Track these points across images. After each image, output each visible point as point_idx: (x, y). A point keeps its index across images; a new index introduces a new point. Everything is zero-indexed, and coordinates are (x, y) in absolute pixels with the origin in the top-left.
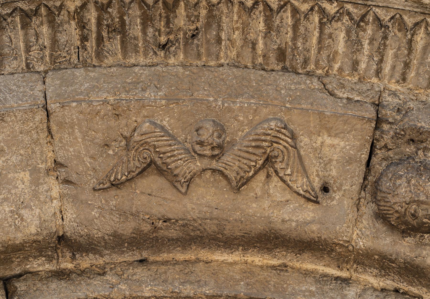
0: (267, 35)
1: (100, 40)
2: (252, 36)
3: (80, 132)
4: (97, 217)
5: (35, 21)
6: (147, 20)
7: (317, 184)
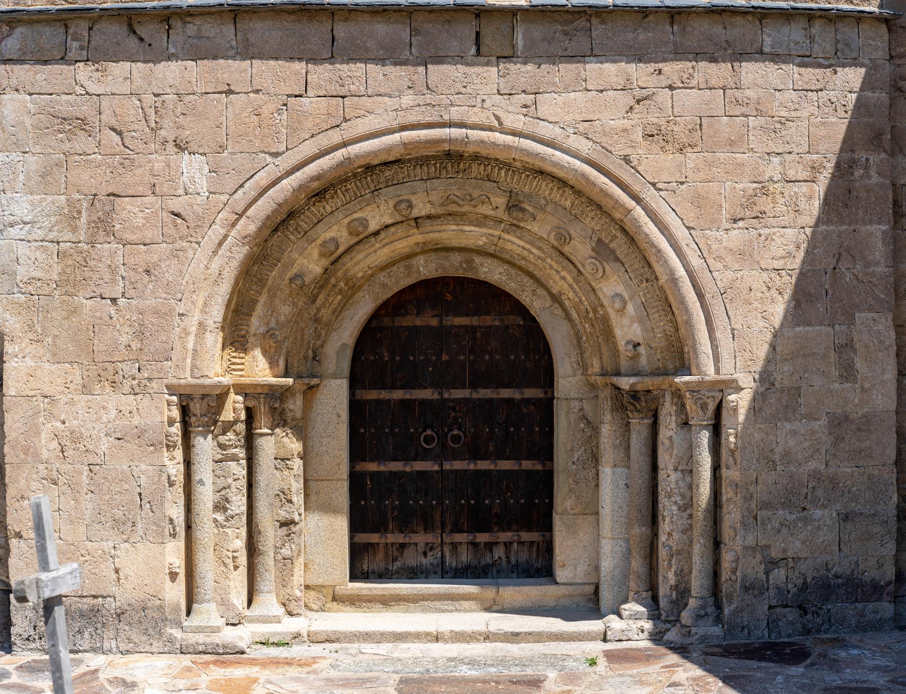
6: (452, 167)
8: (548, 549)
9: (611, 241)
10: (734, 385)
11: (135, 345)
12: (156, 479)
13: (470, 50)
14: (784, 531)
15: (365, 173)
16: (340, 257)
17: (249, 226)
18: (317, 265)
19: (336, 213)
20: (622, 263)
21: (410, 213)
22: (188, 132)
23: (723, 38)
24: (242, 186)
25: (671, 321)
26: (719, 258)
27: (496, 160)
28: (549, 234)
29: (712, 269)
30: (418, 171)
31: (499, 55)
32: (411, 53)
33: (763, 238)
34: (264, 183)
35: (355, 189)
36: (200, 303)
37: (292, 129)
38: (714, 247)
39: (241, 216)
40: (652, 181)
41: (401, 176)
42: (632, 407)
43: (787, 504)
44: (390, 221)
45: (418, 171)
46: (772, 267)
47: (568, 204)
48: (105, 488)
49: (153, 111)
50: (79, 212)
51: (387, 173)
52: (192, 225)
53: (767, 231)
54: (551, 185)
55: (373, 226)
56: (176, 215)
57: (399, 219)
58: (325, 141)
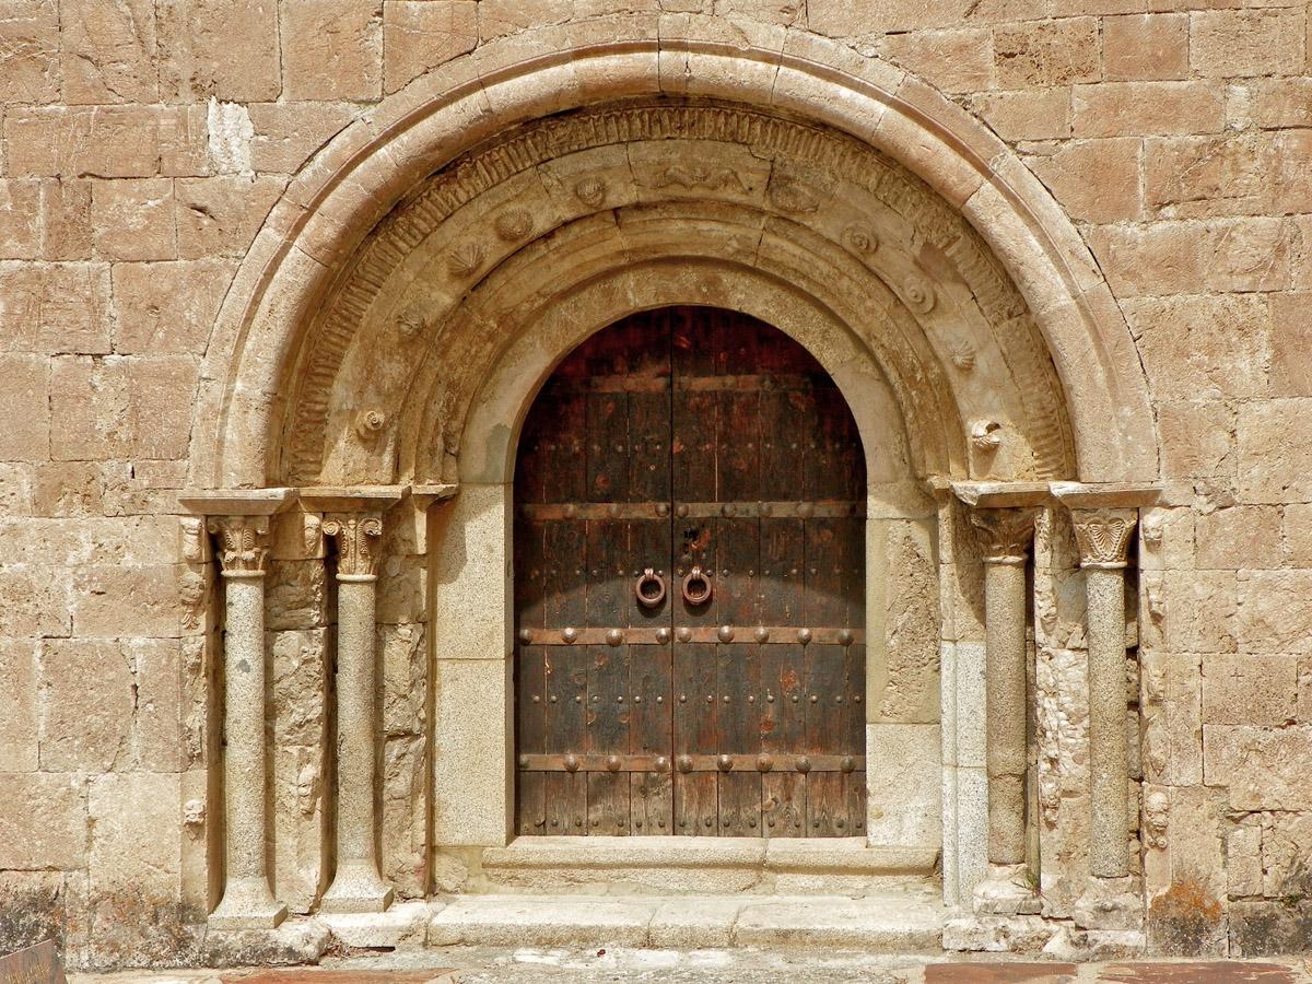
0: (726, 124)
1: (650, 127)
2: (719, 126)
3: (810, 519)
4: (653, 196)
5: (621, 120)
6: (671, 119)
7: (747, 188)
8: (853, 779)
9: (948, 245)
10: (1151, 495)
11: (124, 434)
12: (164, 662)
14: (1255, 760)
15: (523, 132)
16: (487, 277)
17: (324, 228)
19: (475, 203)
20: (967, 285)
21: (603, 201)
22: (216, 64)
24: (310, 159)
25: (1052, 387)
26: (1130, 274)
27: (746, 105)
28: (842, 235)
29: (1117, 294)
30: (613, 126)
33: (1213, 234)
34: (348, 155)
35: (507, 160)
37: (393, 58)
38: (1121, 255)
39: (311, 212)
41: (583, 136)
42: (986, 535)
43: (1258, 714)
44: (569, 216)
45: (613, 126)
46: (1229, 288)
47: (873, 181)
48: (73, 677)
49: (152, 23)
50: (33, 208)
51: (560, 132)
52: (228, 228)
53: (1221, 222)
54: (841, 148)
55: (541, 224)
56: (200, 210)
57: (584, 211)
58: (450, 78)
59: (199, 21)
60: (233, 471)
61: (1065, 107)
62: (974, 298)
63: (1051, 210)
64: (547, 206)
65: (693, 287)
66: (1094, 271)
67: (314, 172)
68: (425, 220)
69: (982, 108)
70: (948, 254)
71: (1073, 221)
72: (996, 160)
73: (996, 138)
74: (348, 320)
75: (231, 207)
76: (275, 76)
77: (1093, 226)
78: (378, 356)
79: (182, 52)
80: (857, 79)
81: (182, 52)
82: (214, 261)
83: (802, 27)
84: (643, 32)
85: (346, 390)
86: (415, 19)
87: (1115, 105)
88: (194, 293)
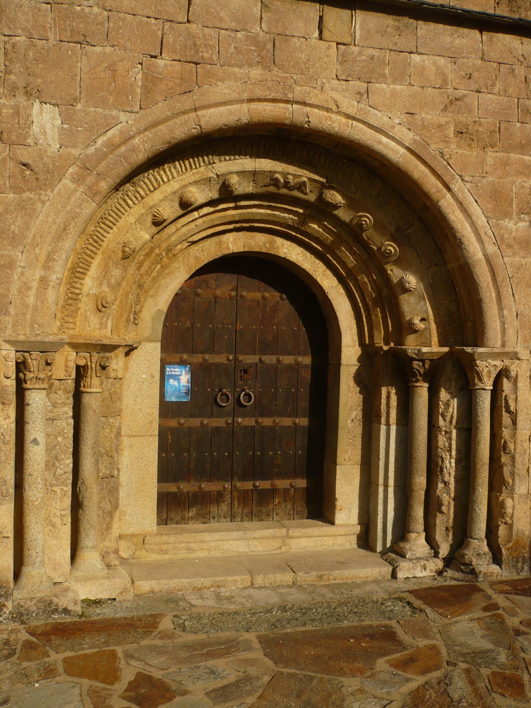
13: (314, 33)
18: (147, 232)
22: (40, 80)
23: (520, 52)
26: (509, 246)
29: (503, 255)
31: (339, 41)
32: (261, 28)
36: (43, 257)
37: (147, 90)
38: (506, 236)
40: (460, 174)
52: (42, 177)
56: (24, 165)
59: (31, 54)
60: (37, 324)
61: (483, 162)
62: (418, 255)
63: (476, 210)
64: (206, 190)
65: (262, 244)
66: (494, 243)
67: (96, 149)
68: (143, 189)
69: (448, 156)
70: (408, 232)
71: (486, 217)
72: (453, 184)
73: (454, 173)
74: (96, 242)
75: (44, 164)
76: (76, 91)
77: (495, 221)
78: (111, 265)
79: (20, 71)
80: (391, 134)
81: (20, 71)
82: (32, 196)
83: (366, 103)
84: (286, 94)
85: (93, 282)
86: (161, 70)
87: (505, 164)
88: (17, 214)
